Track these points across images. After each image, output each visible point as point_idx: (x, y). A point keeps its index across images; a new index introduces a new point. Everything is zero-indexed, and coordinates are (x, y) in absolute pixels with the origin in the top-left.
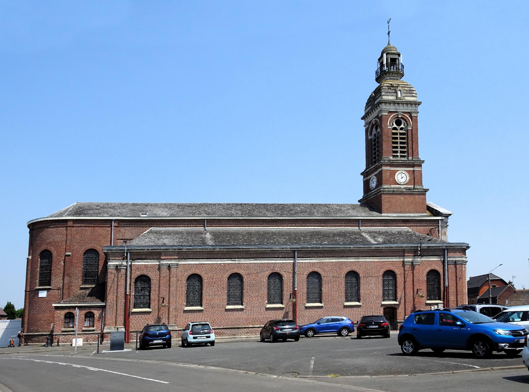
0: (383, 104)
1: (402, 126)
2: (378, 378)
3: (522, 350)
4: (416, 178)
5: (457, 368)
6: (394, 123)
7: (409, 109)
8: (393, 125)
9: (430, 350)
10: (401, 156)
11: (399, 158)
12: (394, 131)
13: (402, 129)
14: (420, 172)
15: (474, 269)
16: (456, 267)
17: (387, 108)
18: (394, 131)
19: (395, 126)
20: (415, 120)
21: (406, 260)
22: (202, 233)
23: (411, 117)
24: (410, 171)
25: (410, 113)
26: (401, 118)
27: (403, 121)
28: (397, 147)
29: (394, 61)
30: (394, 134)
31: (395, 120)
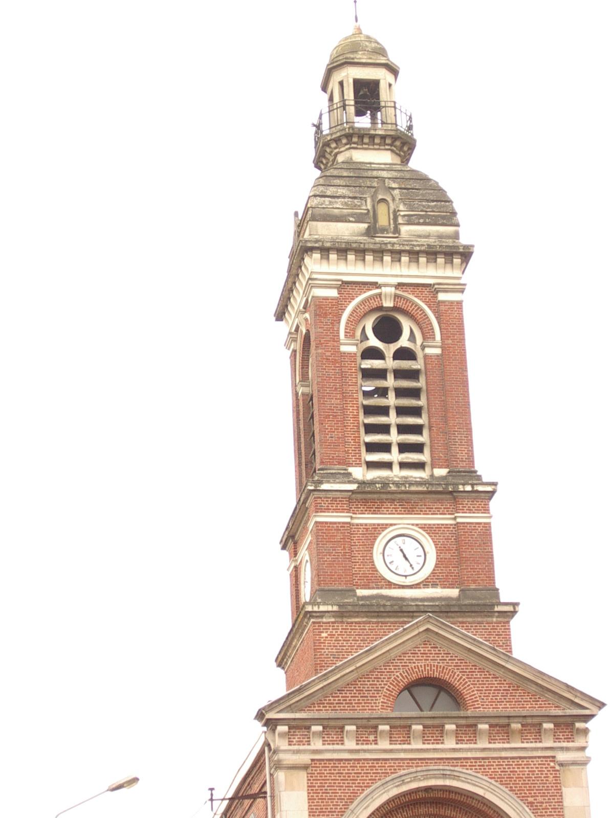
0: (317, 256)
1: (404, 342)
2: (313, 366)
6: (370, 333)
8: (365, 337)
10: (403, 465)
11: (397, 473)
12: (368, 364)
14: (485, 532)
16: (388, 107)
17: (333, 268)
18: (368, 364)
19: (374, 342)
20: (452, 320)
21: (345, 121)
23: (437, 306)
25: (429, 290)
26: (396, 309)
27: (406, 325)
29: (367, 96)
30: (369, 374)
31: (369, 324)
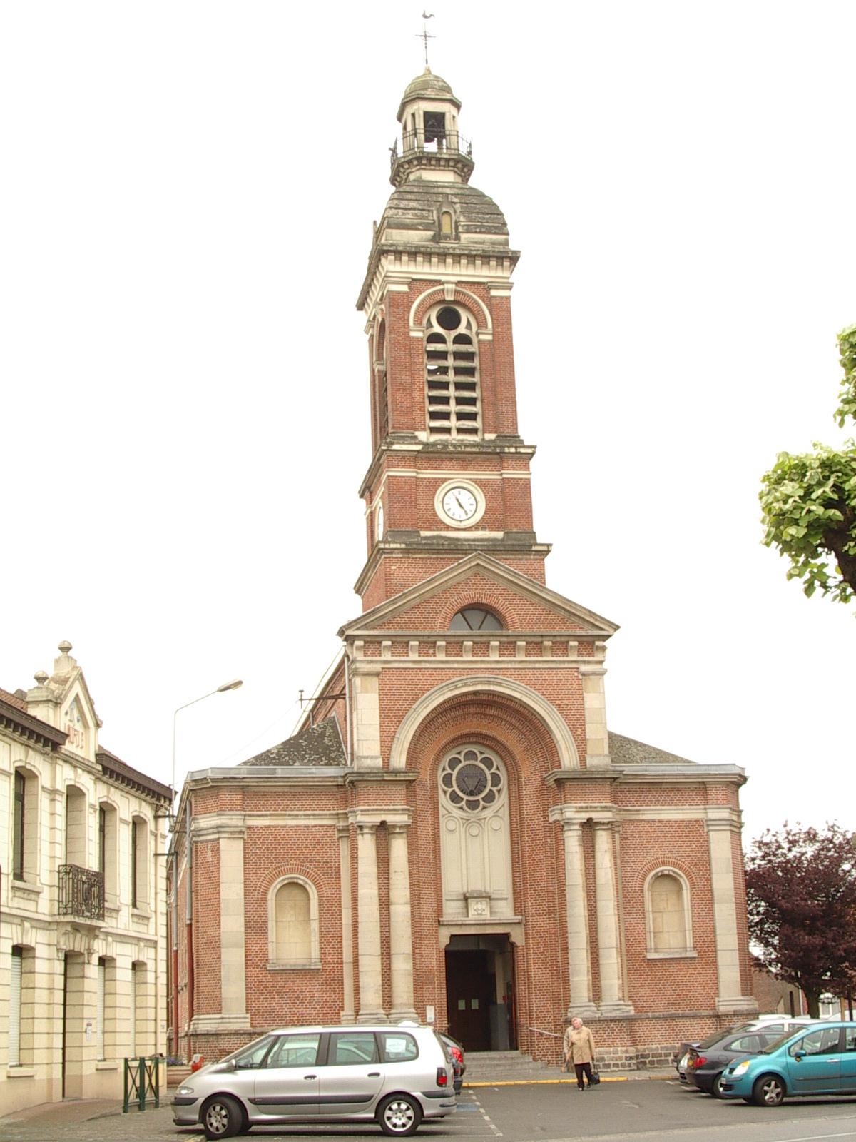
0: (391, 257)
1: (462, 329)
3: (307, 920)
4: (511, 505)
5: (295, 965)
6: (434, 321)
7: (480, 273)
9: (743, 1101)
10: (460, 431)
11: (454, 437)
12: (438, 378)
13: (461, 339)
15: (841, 357)
19: (437, 329)
20: (502, 312)
22: (782, 976)
23: (490, 301)
24: (488, 481)
27: (464, 315)
28: (445, 386)
29: (435, 126)
